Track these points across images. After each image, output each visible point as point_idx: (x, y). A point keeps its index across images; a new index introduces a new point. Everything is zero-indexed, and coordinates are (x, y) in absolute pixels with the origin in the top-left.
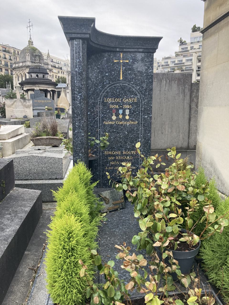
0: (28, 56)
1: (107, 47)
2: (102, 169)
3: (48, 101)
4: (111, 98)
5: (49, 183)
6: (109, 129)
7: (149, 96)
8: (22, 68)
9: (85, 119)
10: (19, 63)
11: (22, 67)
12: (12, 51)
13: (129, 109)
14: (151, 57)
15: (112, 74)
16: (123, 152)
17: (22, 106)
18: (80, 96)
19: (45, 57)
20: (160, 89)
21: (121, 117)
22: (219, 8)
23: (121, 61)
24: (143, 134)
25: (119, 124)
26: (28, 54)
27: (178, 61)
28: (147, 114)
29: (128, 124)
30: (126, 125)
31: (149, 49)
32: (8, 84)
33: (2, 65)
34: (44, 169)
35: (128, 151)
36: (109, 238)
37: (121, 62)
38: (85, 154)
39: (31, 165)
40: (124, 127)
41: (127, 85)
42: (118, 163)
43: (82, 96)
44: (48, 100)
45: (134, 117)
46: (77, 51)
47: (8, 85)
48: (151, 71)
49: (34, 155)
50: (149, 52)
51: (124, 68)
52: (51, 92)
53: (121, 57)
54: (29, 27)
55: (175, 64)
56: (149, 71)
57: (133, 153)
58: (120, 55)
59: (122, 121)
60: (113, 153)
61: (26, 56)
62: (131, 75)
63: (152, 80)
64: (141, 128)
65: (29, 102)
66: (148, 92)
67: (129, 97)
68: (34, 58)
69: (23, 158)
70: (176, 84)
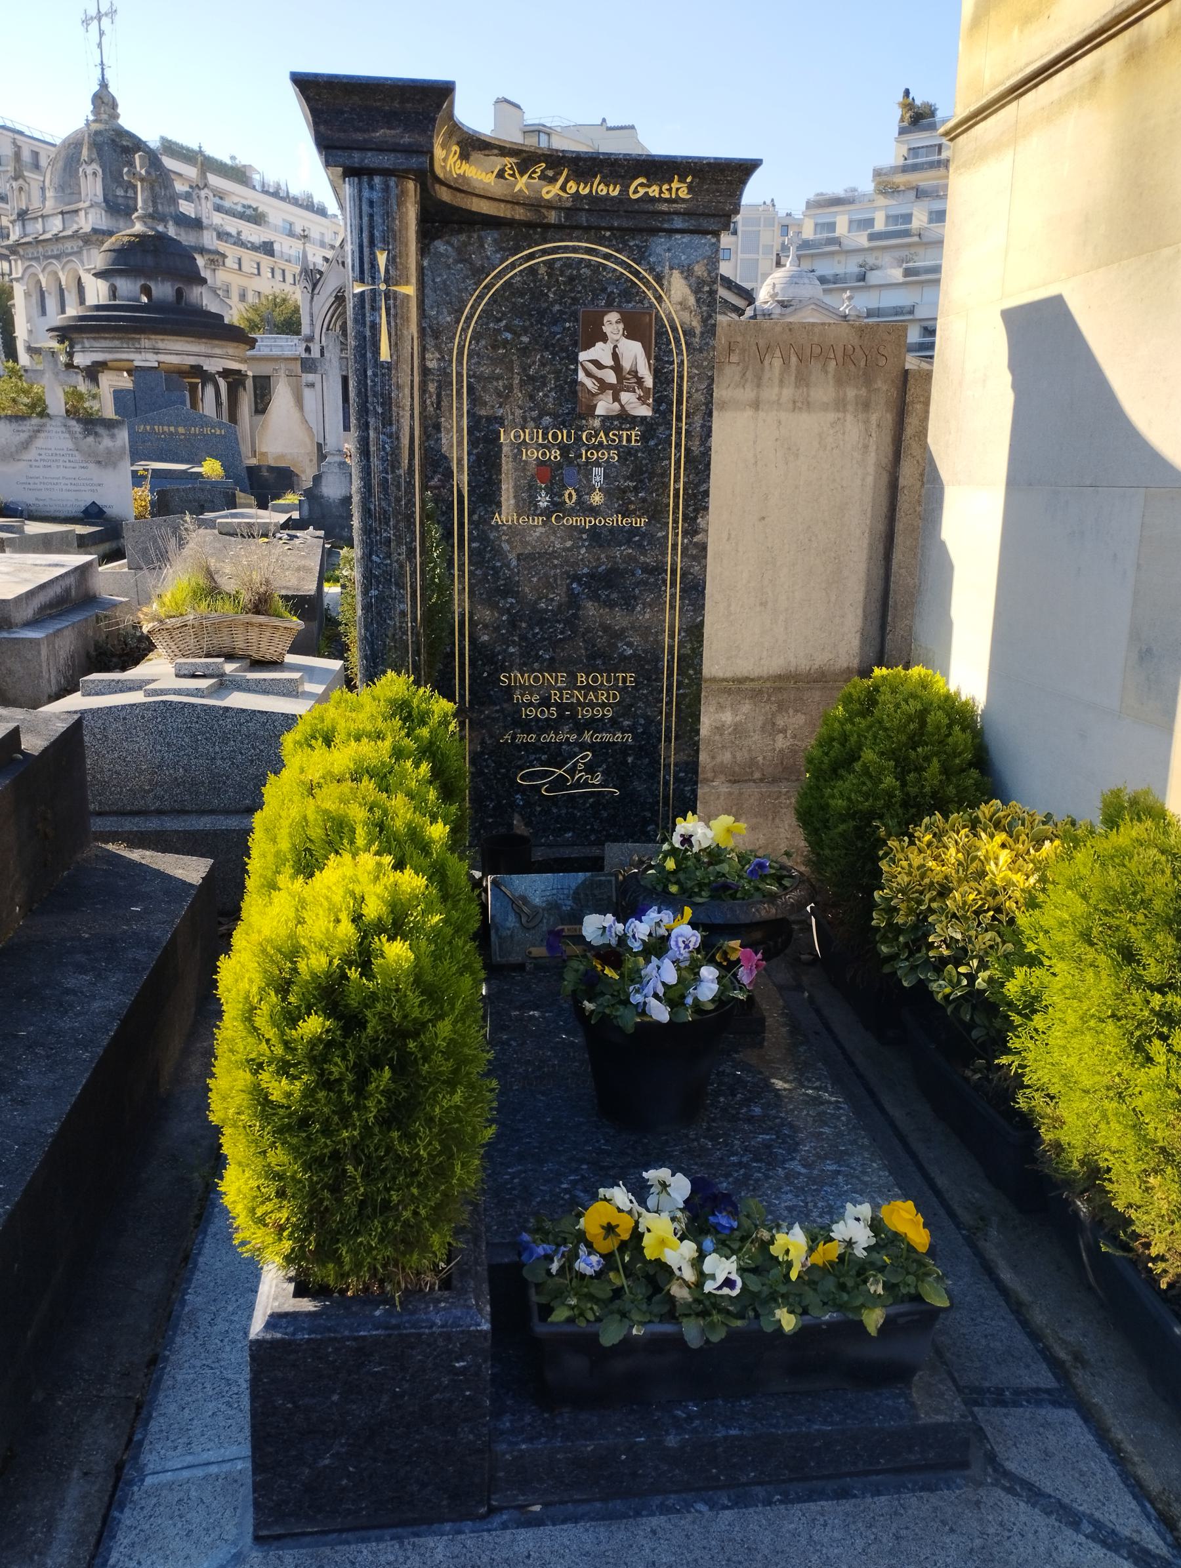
17: (78, 457)
22: (1021, 31)
27: (888, 217)
34: (219, 762)
36: (514, 1043)
44: (204, 421)
46: (377, 234)
54: (96, 22)
55: (873, 237)
61: (82, 180)
65: (113, 436)
68: (126, 192)
70: (830, 376)
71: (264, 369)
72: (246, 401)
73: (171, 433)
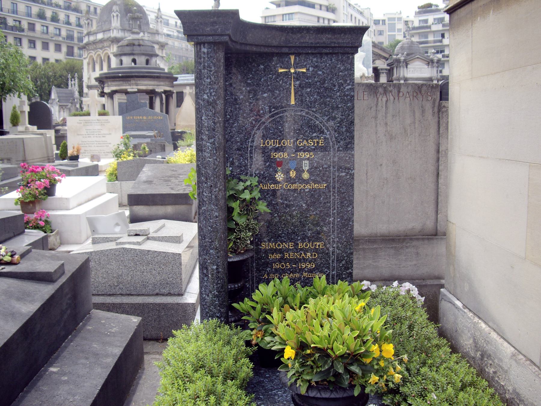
0: (115, 18)
1: (264, 46)
2: (256, 277)
3: (155, 117)
4: (274, 138)
5: (155, 302)
6: (269, 199)
7: (348, 135)
8: (102, 44)
9: (220, 186)
10: (96, 33)
11: (102, 41)
12: (83, 7)
13: (308, 159)
14: (350, 61)
15: (274, 95)
16: (298, 244)
18: (211, 144)
19: (151, 17)
20: (376, 113)
21: (293, 174)
23: (292, 71)
24: (338, 207)
25: (289, 190)
26: (115, 15)
28: (345, 170)
29: (308, 187)
30: (304, 190)
31: (345, 47)
32: (71, 79)
33: (60, 39)
35: (309, 242)
37: (291, 73)
38: (220, 251)
39: (121, 267)
40: (300, 193)
41: (304, 114)
42: (287, 266)
43: (214, 144)
44: (156, 114)
45: (319, 175)
47: (72, 81)
48: (350, 87)
49: (127, 246)
50: (345, 53)
51: (298, 83)
52: (164, 96)
53: (292, 62)
56: (347, 88)
57: (319, 246)
58: (290, 58)
59: (295, 183)
60: (279, 245)
61: (112, 18)
62: (312, 96)
63: (353, 104)
64: (334, 198)
66: (346, 126)
67: (308, 137)
69: (107, 253)
71: (179, 90)
72: (173, 101)
73: (140, 119)
